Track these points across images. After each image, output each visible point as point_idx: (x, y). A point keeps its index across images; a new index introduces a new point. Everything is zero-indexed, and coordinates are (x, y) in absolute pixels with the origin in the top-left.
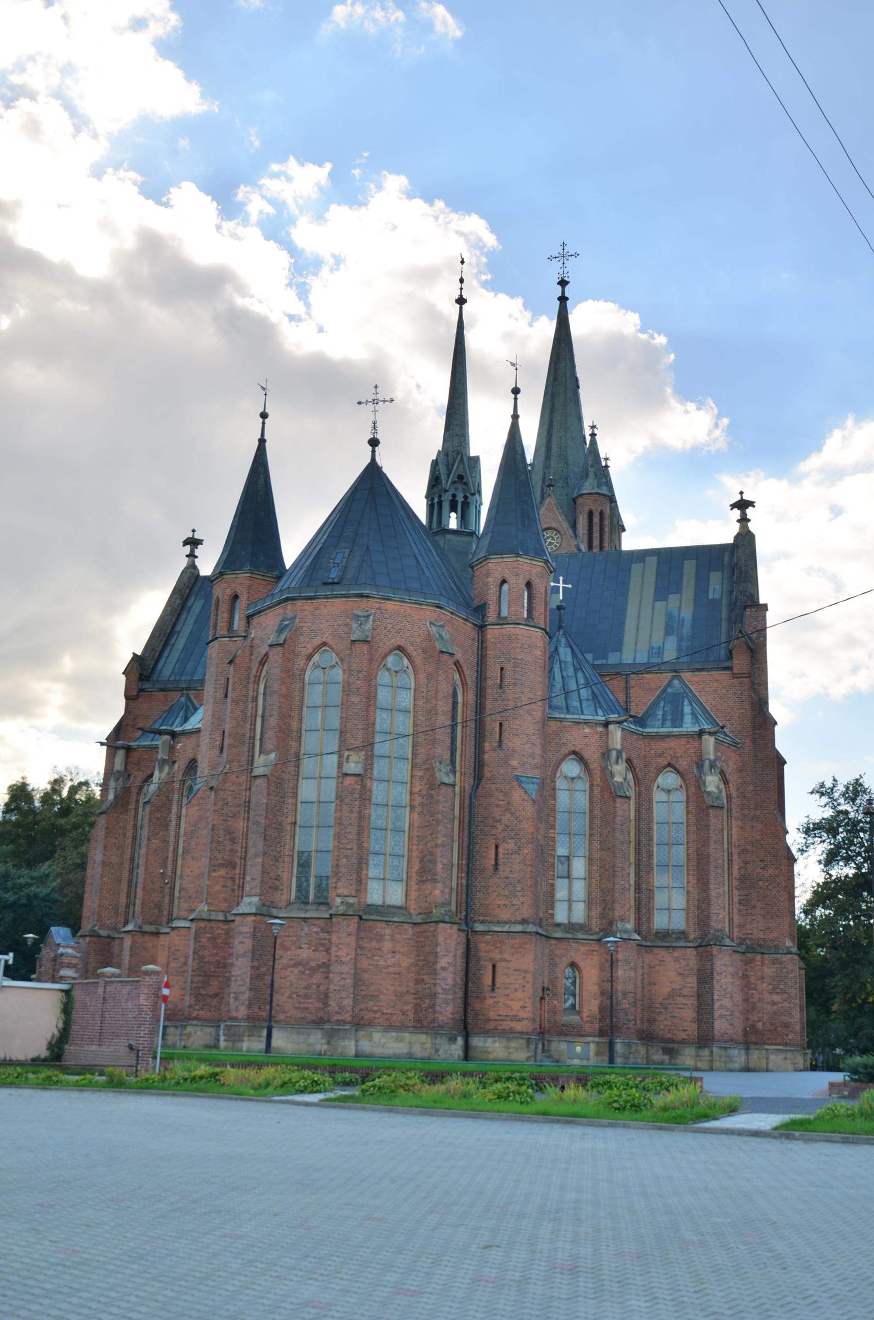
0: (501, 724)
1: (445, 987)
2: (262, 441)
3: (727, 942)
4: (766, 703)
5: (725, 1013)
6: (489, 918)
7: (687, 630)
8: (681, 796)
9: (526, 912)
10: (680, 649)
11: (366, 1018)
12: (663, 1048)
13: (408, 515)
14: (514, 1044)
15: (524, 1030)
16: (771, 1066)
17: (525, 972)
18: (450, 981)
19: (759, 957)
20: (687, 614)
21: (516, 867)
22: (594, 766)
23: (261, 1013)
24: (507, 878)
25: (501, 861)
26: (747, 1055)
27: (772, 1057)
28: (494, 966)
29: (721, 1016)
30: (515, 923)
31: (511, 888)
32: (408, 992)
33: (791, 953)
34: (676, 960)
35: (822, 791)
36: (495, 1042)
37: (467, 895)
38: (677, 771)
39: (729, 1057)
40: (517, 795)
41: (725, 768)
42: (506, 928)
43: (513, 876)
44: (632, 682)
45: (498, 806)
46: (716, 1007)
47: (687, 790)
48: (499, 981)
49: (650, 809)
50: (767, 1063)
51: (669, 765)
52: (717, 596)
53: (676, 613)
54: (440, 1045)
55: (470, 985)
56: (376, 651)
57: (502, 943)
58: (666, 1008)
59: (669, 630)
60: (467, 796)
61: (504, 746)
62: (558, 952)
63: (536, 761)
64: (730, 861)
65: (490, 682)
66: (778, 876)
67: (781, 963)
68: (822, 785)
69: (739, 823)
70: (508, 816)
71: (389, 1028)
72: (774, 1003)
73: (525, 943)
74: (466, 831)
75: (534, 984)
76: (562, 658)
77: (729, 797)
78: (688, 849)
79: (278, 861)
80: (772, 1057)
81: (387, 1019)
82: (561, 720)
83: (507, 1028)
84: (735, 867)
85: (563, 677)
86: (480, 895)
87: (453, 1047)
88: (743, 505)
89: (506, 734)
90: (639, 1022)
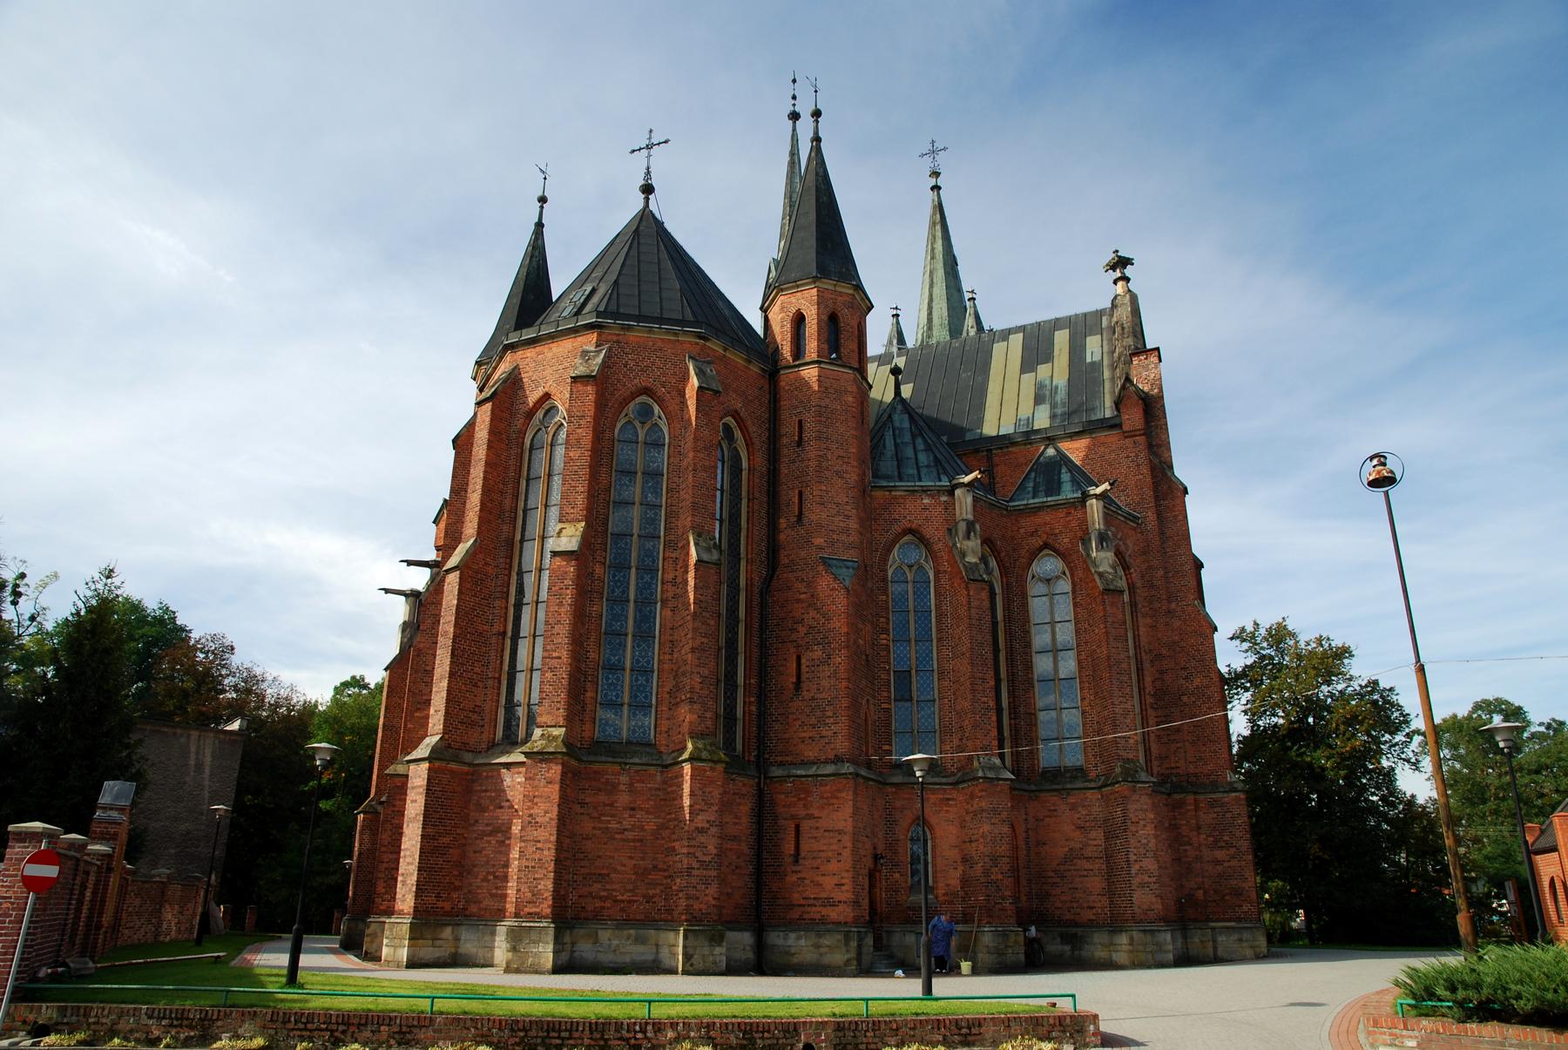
0: (800, 494)
1: (702, 858)
2: (540, 225)
3: (1143, 776)
4: (1171, 467)
5: (1146, 879)
6: (789, 759)
7: (1061, 395)
8: (1065, 586)
9: (842, 745)
10: (1053, 417)
11: (590, 908)
12: (1061, 935)
13: (690, 272)
14: (826, 941)
15: (842, 919)
16: (1220, 953)
17: (840, 832)
18: (712, 849)
19: (1190, 798)
20: (1061, 380)
21: (825, 683)
22: (938, 546)
23: (440, 904)
24: (813, 699)
25: (804, 676)
26: (1185, 937)
27: (1221, 939)
28: (797, 827)
29: (1142, 885)
30: (826, 762)
31: (819, 713)
32: (655, 867)
33: (1236, 791)
34: (1073, 808)
35: (1240, 636)
36: (799, 938)
37: (759, 727)
38: (1058, 553)
39: (1157, 944)
40: (824, 583)
41: (1123, 548)
42: (812, 771)
43: (823, 695)
44: (996, 460)
45: (799, 601)
46: (1135, 868)
47: (1072, 575)
48: (804, 847)
49: (1025, 605)
50: (1215, 948)
51: (1046, 546)
52: (1097, 358)
53: (1048, 382)
54: (695, 948)
55: (765, 855)
56: (612, 394)
57: (808, 792)
58: (1062, 877)
59: (1038, 400)
60: (756, 591)
61: (805, 520)
62: (898, 804)
63: (851, 539)
64: (1140, 671)
65: (785, 441)
66: (1208, 687)
67: (1222, 806)
68: (1243, 630)
69: (1148, 620)
70: (812, 613)
71: (626, 922)
72: (1217, 862)
73: (839, 791)
74: (756, 640)
75: (855, 850)
76: (897, 424)
77: (1132, 587)
78: (1079, 654)
79: (476, 685)
80: (1221, 939)
81: (622, 910)
82: (890, 489)
83: (818, 916)
84: (1148, 679)
85: (896, 445)
86: (777, 727)
87: (718, 950)
88: (1121, 262)
89: (807, 505)
90: (1024, 898)
